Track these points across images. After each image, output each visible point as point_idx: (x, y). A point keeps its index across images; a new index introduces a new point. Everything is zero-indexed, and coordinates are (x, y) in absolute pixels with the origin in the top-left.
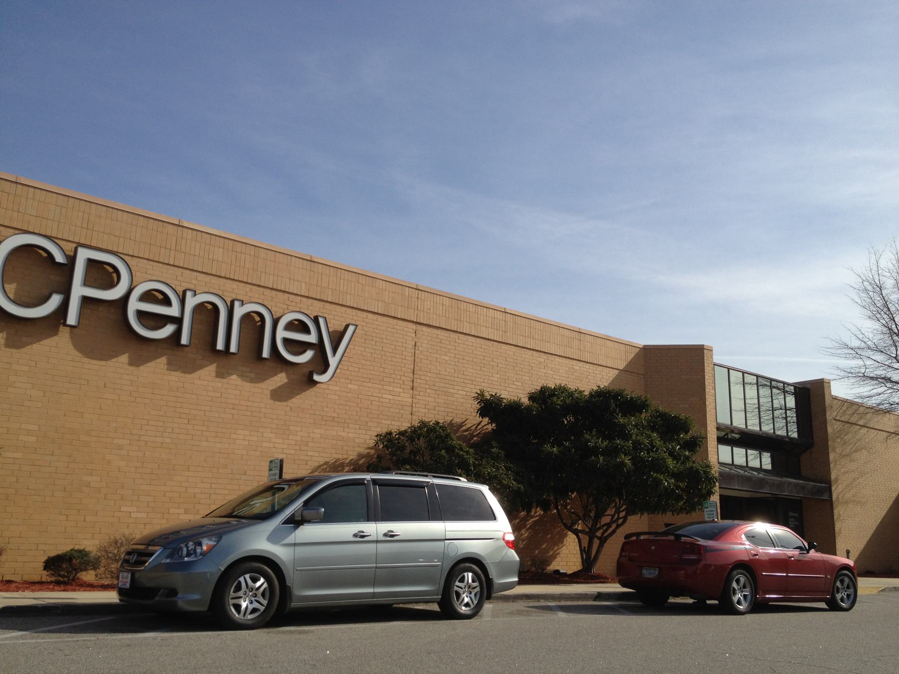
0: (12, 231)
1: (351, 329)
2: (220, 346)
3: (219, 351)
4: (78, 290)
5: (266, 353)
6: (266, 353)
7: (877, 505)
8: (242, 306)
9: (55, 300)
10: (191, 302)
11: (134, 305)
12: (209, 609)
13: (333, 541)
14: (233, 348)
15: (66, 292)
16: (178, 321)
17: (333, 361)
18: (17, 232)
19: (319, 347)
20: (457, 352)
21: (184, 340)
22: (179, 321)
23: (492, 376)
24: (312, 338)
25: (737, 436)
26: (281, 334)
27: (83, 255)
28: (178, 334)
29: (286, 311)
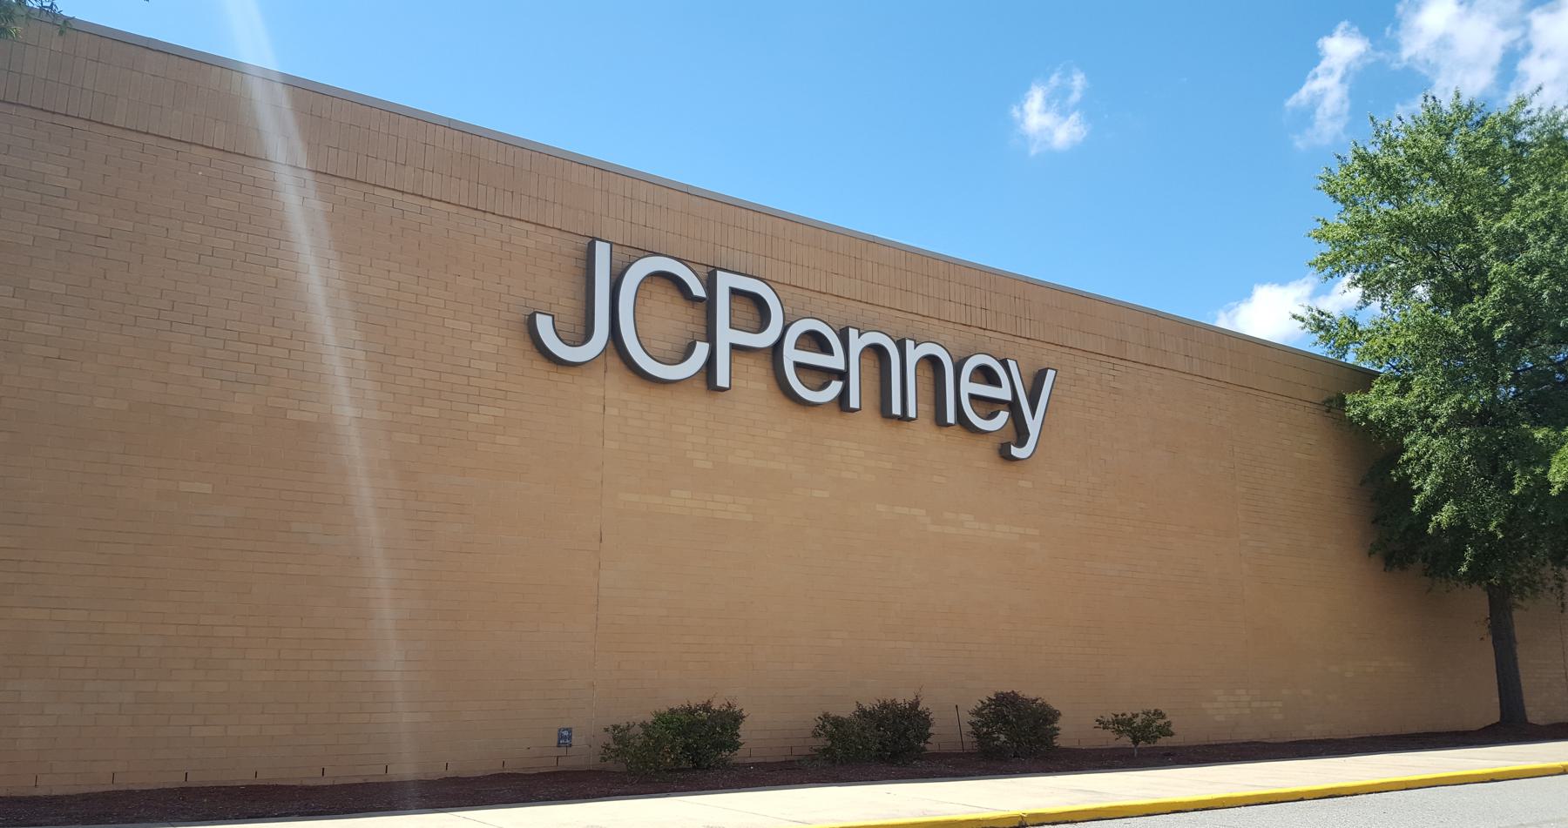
0: (641, 253)
1: (1050, 374)
2: (896, 409)
3: (895, 417)
4: (726, 336)
5: (951, 417)
6: (951, 417)
7: (1464, 372)
8: (915, 348)
9: (702, 349)
10: (857, 343)
11: (791, 355)
12: (1501, 719)
13: (267, 777)
14: (912, 413)
15: (711, 338)
16: (843, 376)
17: (1033, 425)
18: (646, 253)
19: (1013, 406)
20: (1112, 372)
21: (854, 402)
22: (843, 376)
23: (1084, 400)
24: (1004, 393)
25: (1406, 441)
26: (968, 388)
27: (725, 282)
28: (844, 396)
29: (633, 259)
